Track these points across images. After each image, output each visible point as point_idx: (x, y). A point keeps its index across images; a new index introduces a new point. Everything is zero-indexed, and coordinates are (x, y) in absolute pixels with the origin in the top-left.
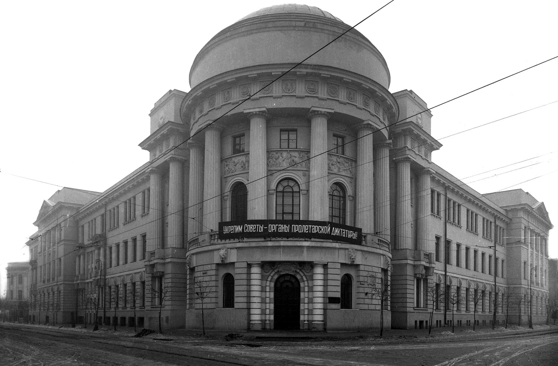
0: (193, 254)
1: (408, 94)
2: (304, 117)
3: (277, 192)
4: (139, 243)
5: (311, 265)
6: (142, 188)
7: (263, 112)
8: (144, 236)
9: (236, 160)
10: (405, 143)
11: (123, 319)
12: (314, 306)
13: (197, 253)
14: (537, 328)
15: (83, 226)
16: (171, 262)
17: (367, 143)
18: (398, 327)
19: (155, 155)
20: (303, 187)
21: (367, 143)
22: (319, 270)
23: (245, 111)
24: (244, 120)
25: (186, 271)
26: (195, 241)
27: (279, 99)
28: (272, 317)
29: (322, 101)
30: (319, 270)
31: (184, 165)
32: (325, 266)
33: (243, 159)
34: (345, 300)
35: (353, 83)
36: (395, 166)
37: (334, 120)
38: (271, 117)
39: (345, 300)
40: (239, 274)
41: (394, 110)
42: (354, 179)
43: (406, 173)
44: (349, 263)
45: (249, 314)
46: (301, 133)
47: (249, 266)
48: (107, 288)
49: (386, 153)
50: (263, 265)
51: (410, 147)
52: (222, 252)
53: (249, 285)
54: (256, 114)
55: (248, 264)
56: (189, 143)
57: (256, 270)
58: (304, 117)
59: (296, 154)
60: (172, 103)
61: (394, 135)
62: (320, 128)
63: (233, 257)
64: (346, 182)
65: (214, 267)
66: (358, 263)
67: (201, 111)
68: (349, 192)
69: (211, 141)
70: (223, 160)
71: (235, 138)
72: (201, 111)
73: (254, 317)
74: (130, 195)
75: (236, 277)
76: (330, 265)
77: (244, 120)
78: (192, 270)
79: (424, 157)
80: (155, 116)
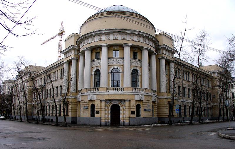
0: (80, 96)
1: (163, 34)
2: (121, 47)
3: (112, 73)
4: (59, 89)
5: (124, 101)
6: (61, 68)
7: (106, 45)
8: (61, 87)
9: (96, 61)
10: (163, 52)
11: (49, 119)
12: (125, 116)
13: (81, 96)
14: (19, 120)
15: (36, 81)
16: (71, 98)
17: (145, 54)
18: (74, 121)
19: (66, 56)
20: (121, 71)
21: (145, 54)
22: (127, 102)
23: (100, 45)
24: (100, 48)
25: (77, 102)
26: (81, 91)
27: (112, 39)
28: (110, 121)
29: (128, 40)
30: (127, 102)
31: (77, 61)
32: (130, 101)
33: (99, 61)
34: (137, 112)
35: (139, 34)
36: (158, 61)
37: (132, 47)
38: (110, 47)
39: (137, 112)
40: (97, 103)
41: (156, 42)
42: (141, 67)
43: (163, 62)
44: (139, 100)
45: (101, 119)
46: (121, 51)
47: (101, 101)
48: (46, 106)
49: (154, 58)
50: (106, 101)
51: (164, 53)
52: (91, 96)
53: (101, 106)
54: (104, 46)
55: (100, 101)
56: (79, 54)
57: (103, 102)
58: (121, 47)
59: (119, 59)
60: (74, 38)
61: (157, 50)
62: (127, 50)
63: (95, 98)
64: (99, 69)
65: (88, 101)
66: (143, 100)
67: (84, 44)
68: (139, 73)
69: (87, 54)
70: (92, 61)
71: (96, 53)
72: (84, 44)
73: (102, 121)
74: (56, 70)
75: (96, 105)
76: (131, 101)
77: (100, 48)
78: (80, 102)
79: (171, 56)
80: (66, 42)
